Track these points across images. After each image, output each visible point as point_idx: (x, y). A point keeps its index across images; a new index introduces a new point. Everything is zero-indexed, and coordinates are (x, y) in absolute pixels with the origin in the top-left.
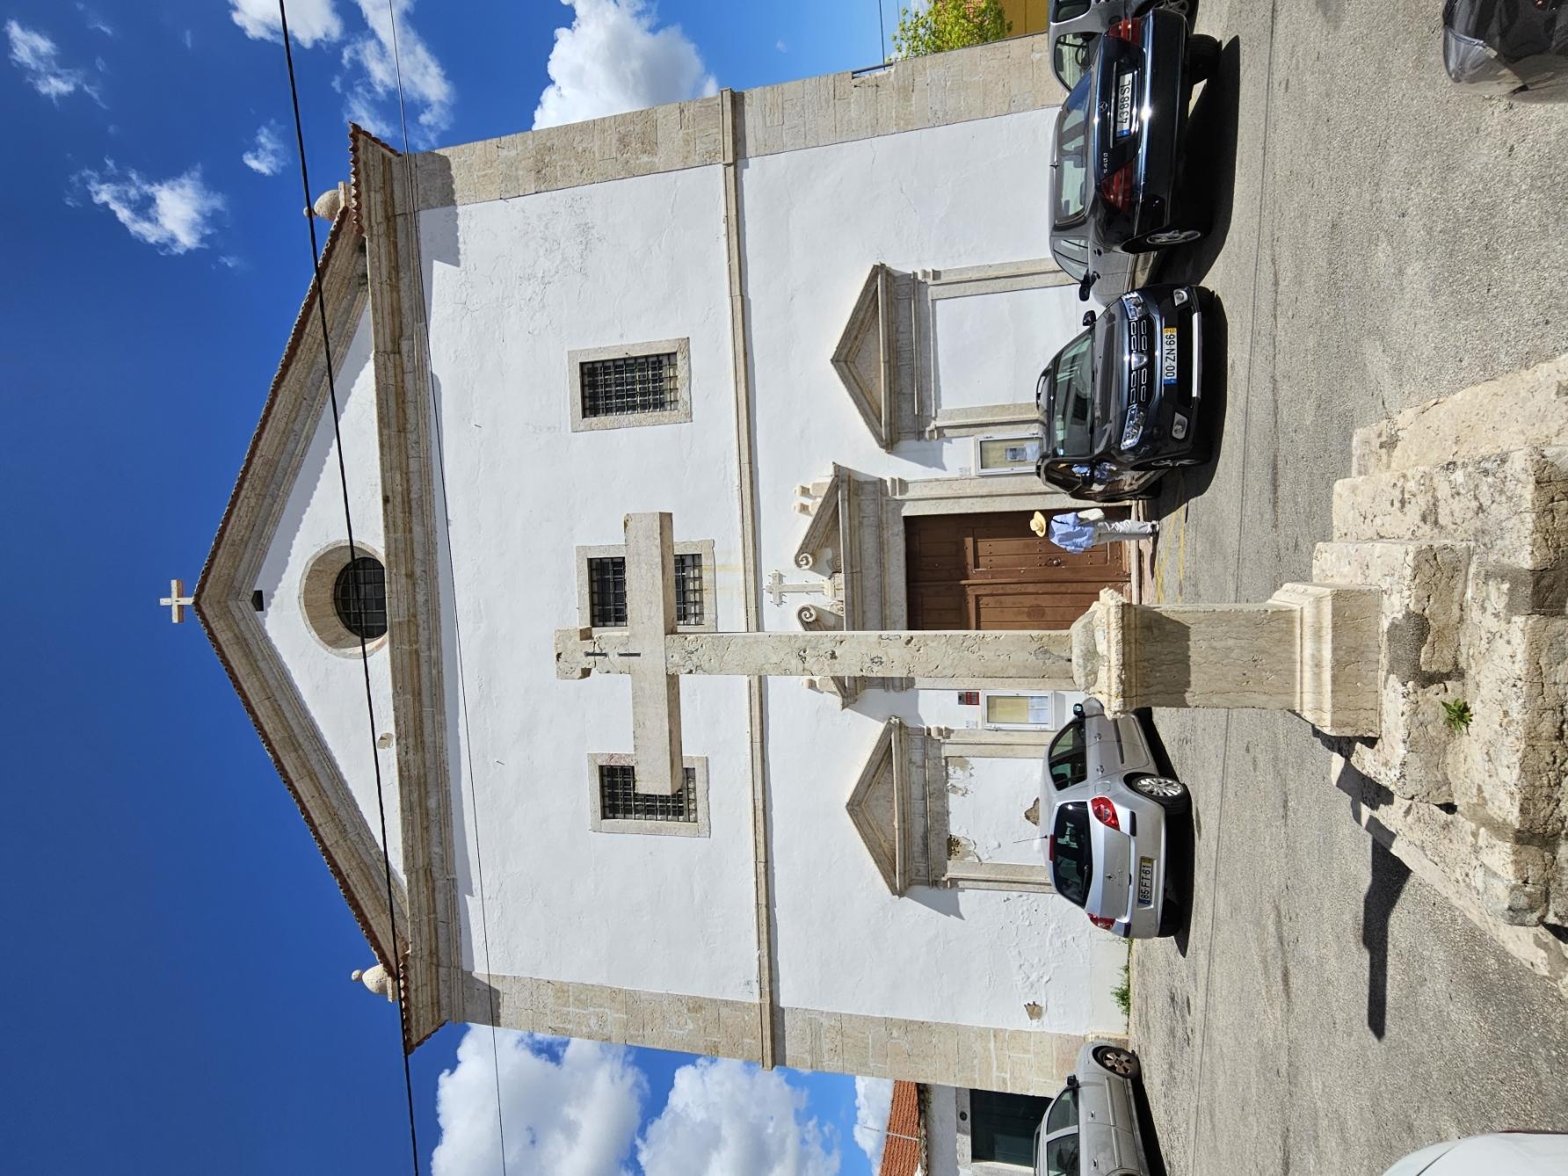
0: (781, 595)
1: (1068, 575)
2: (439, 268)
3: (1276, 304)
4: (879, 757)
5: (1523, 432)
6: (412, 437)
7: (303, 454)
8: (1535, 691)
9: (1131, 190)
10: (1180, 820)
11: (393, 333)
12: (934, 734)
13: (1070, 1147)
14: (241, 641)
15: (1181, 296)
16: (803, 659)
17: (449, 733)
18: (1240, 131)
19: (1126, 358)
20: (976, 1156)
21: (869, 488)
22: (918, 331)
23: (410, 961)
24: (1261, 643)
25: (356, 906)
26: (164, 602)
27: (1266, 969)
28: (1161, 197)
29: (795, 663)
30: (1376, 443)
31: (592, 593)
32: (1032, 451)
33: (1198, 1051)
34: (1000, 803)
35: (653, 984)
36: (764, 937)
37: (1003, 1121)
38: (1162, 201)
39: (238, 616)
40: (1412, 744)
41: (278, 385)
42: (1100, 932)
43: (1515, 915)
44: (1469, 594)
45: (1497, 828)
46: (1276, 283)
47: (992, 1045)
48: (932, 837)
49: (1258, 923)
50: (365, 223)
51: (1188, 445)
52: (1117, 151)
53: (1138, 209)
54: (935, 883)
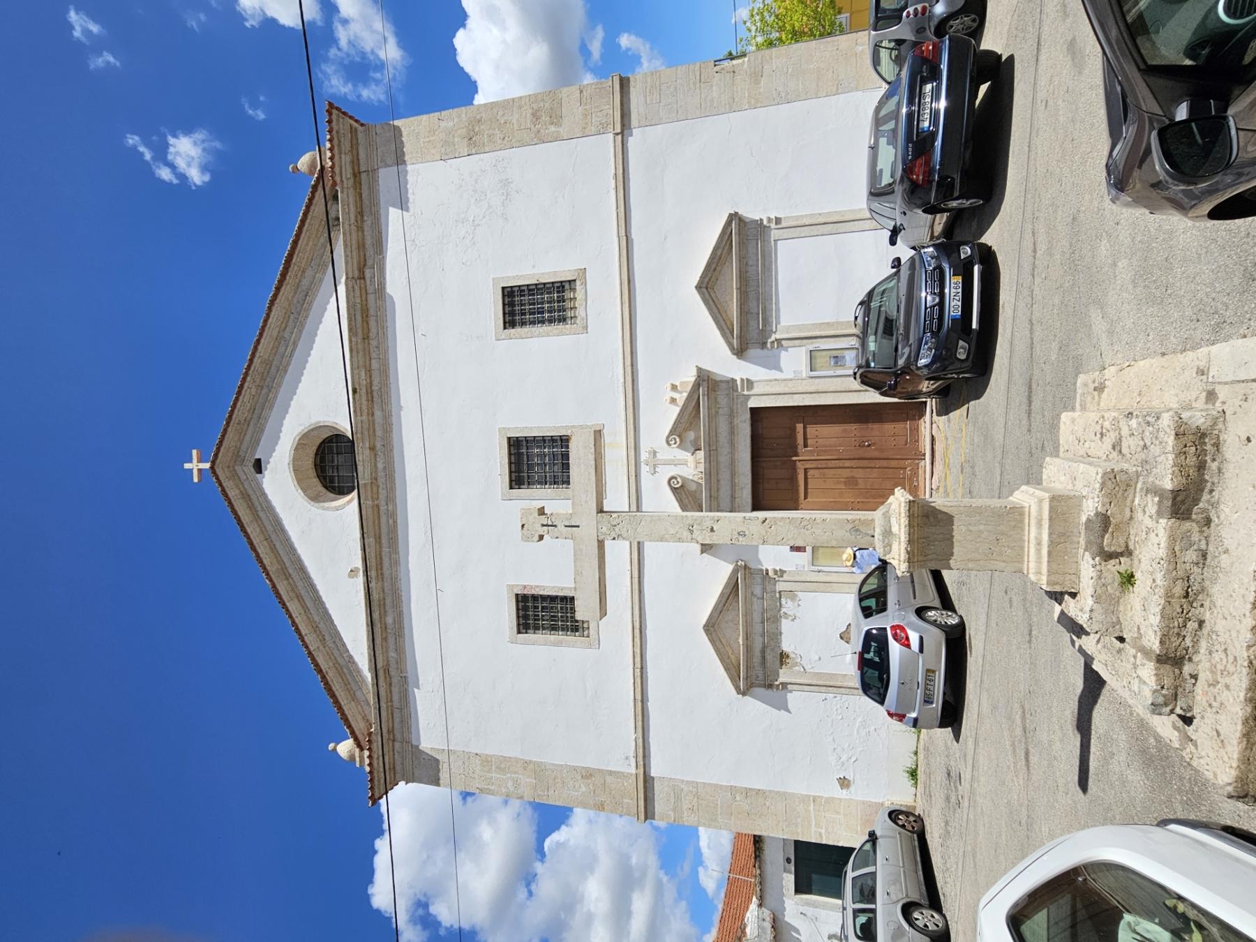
0: (655, 466)
1: (876, 454)
2: (394, 214)
3: (1034, 267)
4: (729, 591)
5: (1177, 395)
6: (374, 343)
7: (291, 356)
8: (1171, 568)
9: (929, 172)
10: (956, 642)
11: (359, 263)
12: (771, 574)
13: (870, 882)
14: (246, 497)
15: (966, 251)
16: (692, 532)
17: (402, 568)
18: (1014, 128)
19: (923, 294)
20: (799, 889)
21: (724, 386)
22: (764, 265)
23: (374, 737)
24: (1002, 528)
25: (333, 696)
26: (187, 466)
27: (1014, 751)
28: (955, 167)
29: (686, 534)
30: (1092, 386)
31: (510, 463)
32: (851, 360)
33: (965, 811)
34: (821, 628)
35: (556, 756)
36: (640, 724)
37: (819, 866)
38: (953, 179)
39: (243, 477)
40: (1097, 598)
41: (272, 303)
42: (894, 723)
43: (1156, 708)
44: (1137, 502)
45: (1146, 652)
46: (1035, 251)
47: (812, 808)
48: (768, 651)
49: (1010, 718)
50: (338, 179)
51: (969, 364)
52: (918, 144)
53: (935, 184)
54: (770, 686)
